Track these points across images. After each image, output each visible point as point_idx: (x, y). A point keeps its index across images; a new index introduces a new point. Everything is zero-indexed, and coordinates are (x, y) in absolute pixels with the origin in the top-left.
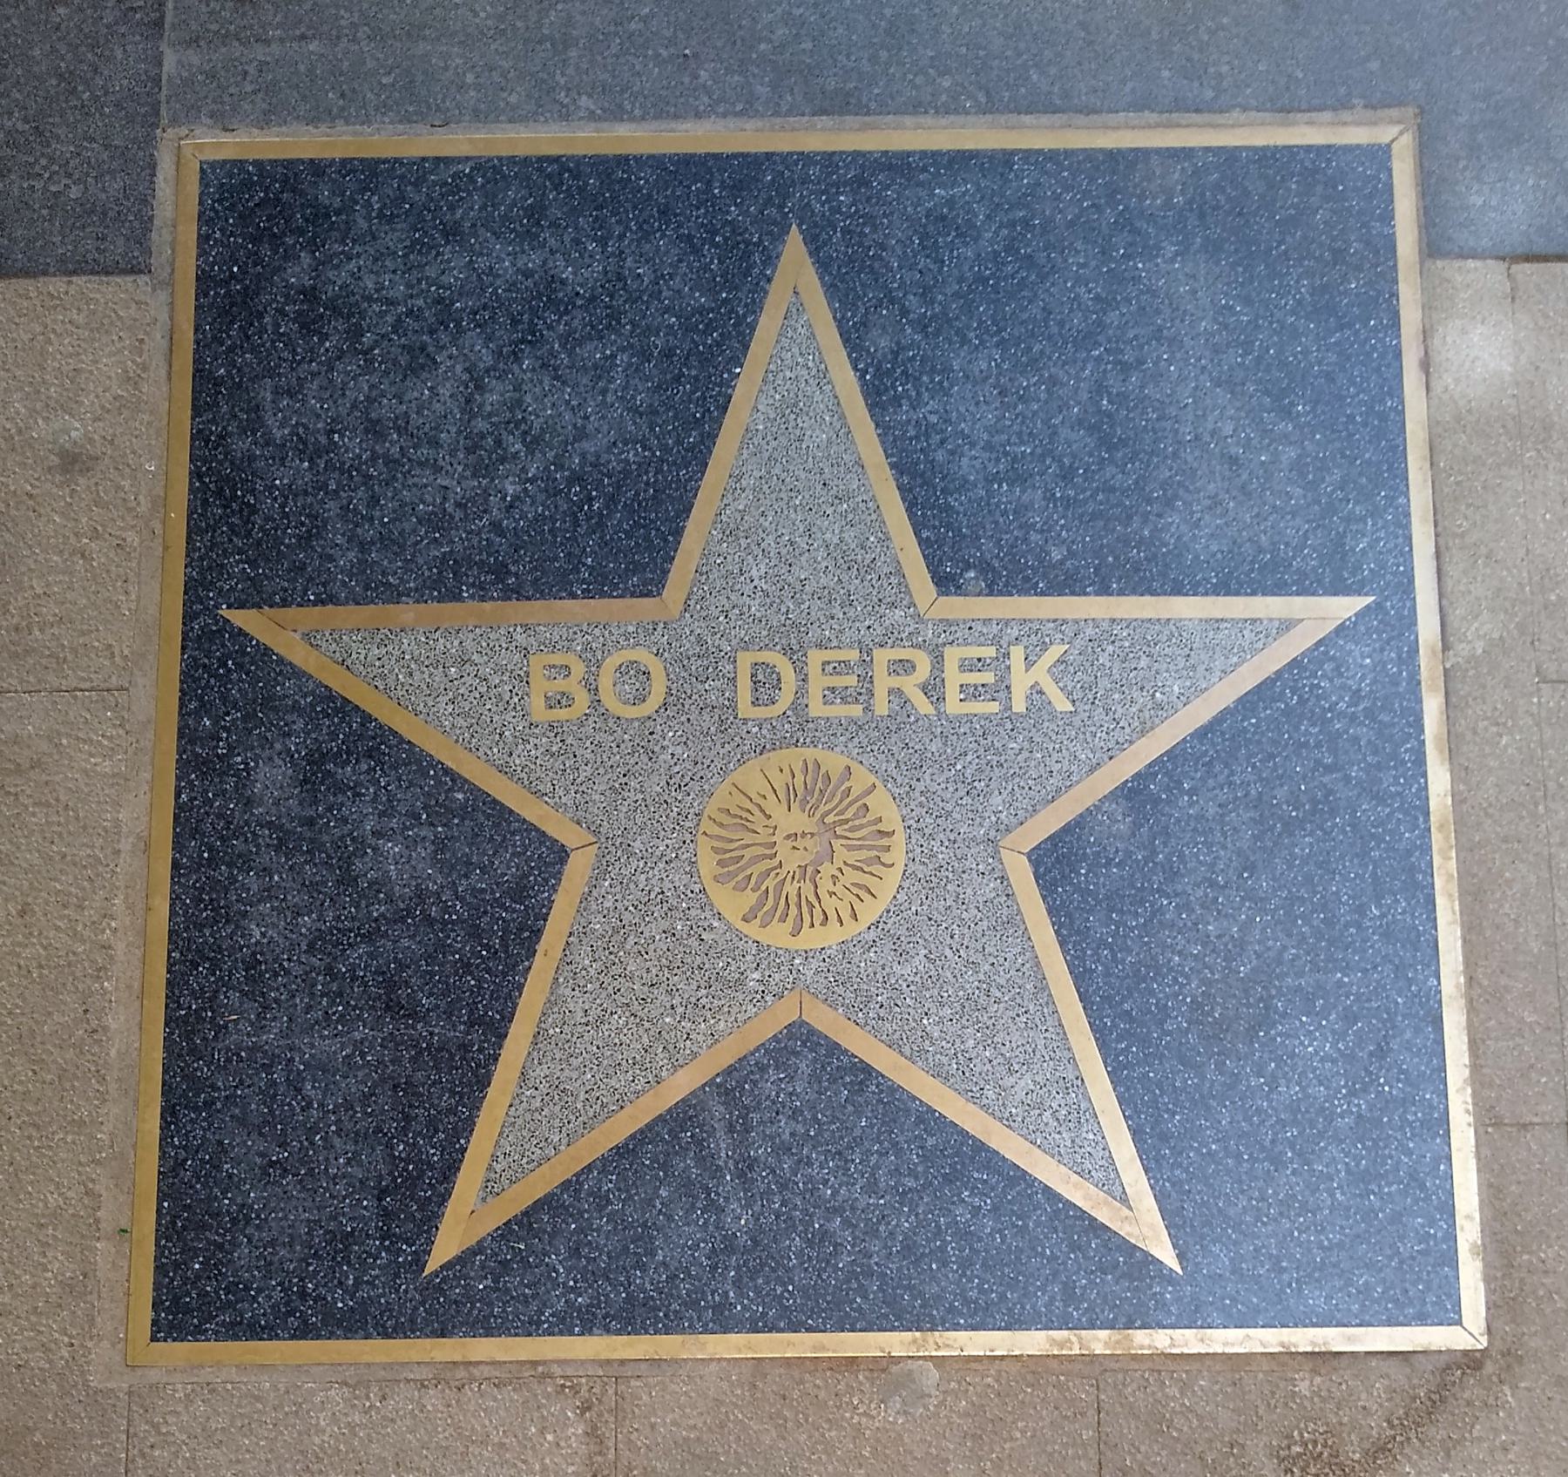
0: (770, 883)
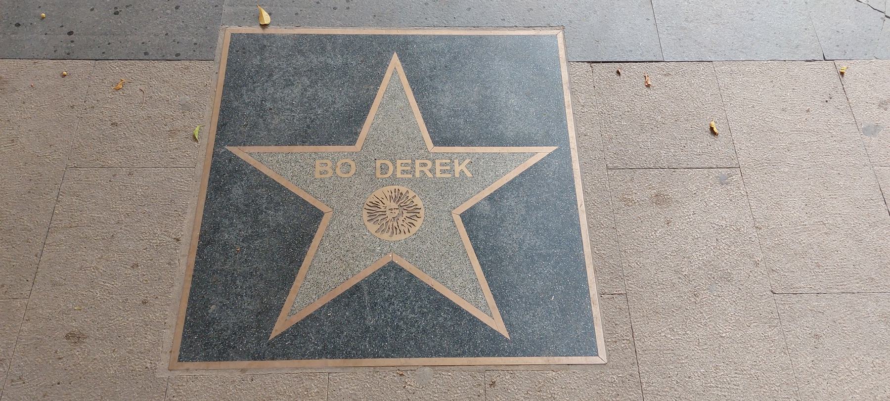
0: (384, 222)
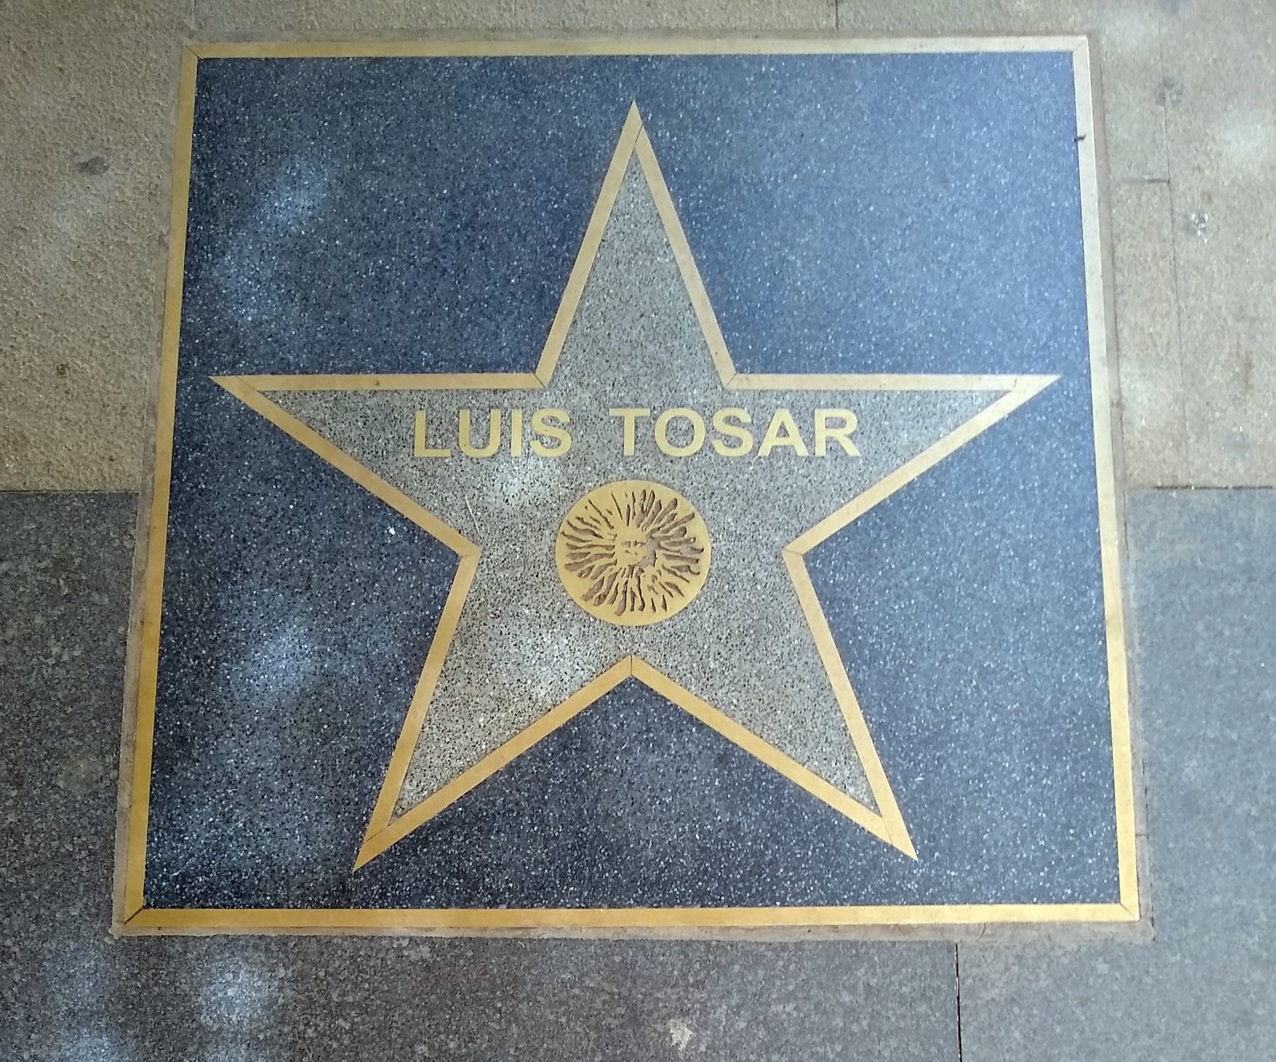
0: (607, 574)
